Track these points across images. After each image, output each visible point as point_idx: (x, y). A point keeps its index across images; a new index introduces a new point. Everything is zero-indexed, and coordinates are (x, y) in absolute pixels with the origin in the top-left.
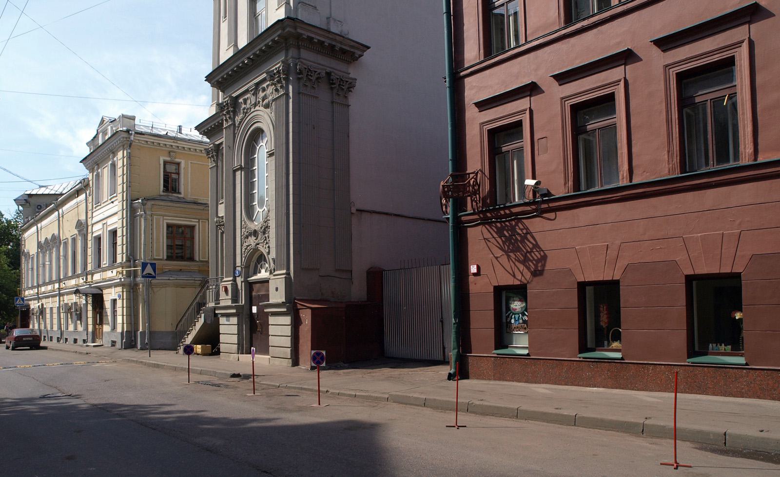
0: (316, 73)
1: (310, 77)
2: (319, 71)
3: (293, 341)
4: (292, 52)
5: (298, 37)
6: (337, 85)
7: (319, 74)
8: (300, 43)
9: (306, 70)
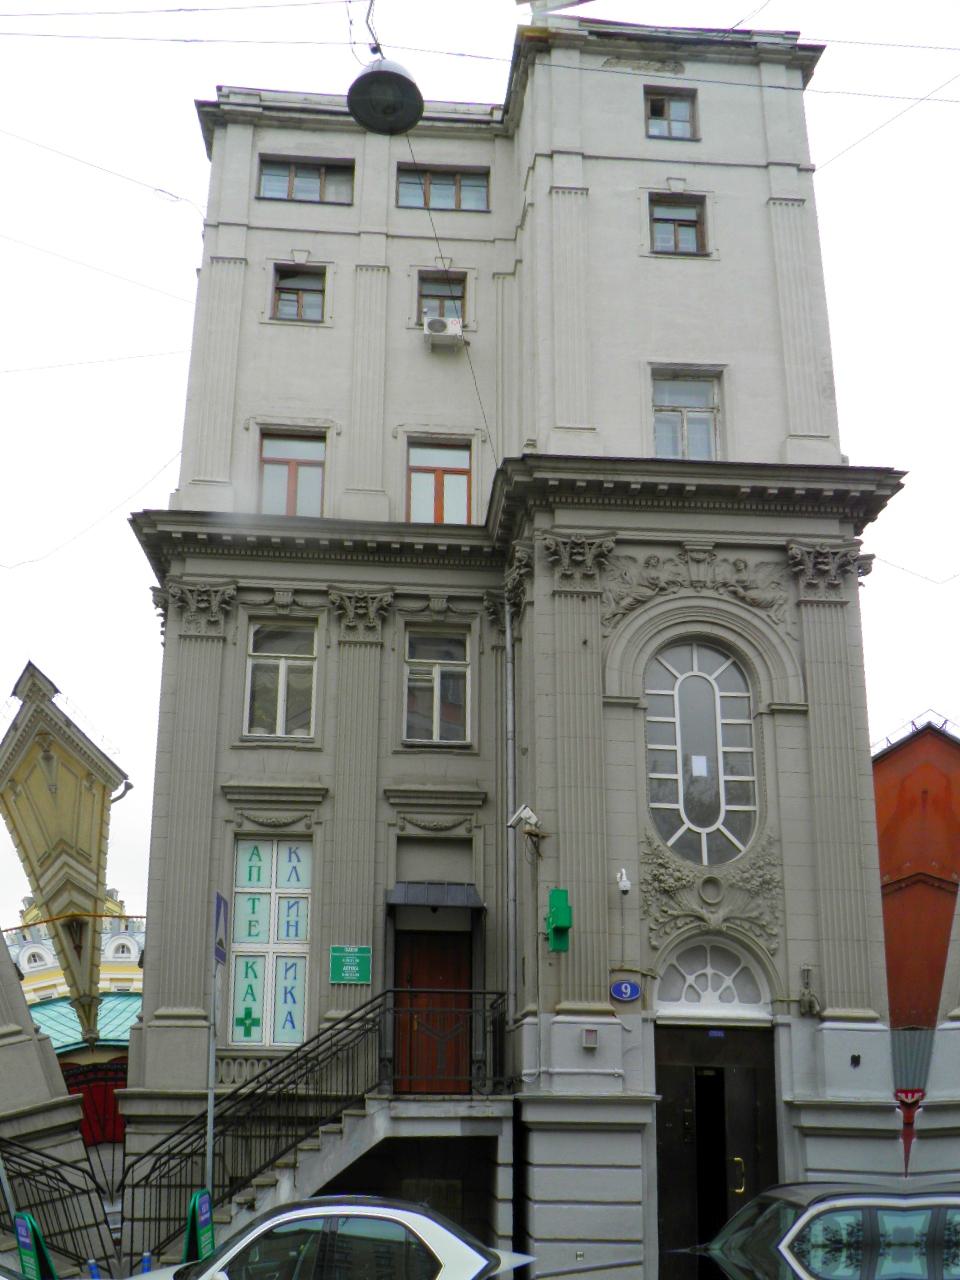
5: (542, 488)
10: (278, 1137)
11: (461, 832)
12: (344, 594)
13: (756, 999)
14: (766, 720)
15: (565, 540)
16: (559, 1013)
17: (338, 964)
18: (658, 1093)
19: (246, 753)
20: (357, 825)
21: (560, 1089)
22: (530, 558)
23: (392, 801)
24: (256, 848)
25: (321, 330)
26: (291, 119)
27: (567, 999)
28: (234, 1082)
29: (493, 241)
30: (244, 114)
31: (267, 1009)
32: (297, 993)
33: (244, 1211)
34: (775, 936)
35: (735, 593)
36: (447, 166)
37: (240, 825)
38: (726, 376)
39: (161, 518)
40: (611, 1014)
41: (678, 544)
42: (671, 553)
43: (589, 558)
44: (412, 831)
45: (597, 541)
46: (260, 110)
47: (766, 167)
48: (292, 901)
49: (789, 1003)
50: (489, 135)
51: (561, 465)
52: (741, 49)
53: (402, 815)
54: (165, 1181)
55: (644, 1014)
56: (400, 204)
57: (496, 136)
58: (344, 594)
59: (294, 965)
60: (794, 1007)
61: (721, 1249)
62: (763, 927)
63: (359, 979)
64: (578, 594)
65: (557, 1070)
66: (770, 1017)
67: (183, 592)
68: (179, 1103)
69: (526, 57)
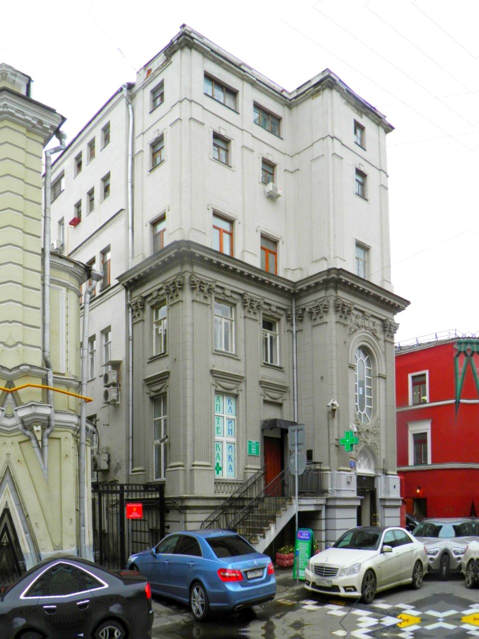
0: (208, 285)
1: (202, 288)
2: (210, 283)
3: (285, 444)
4: (187, 268)
6: (248, 304)
7: (210, 285)
8: (193, 260)
9: (199, 282)
10: (235, 514)
11: (280, 401)
12: (311, 307)
13: (370, 468)
14: (378, 379)
16: (339, 470)
17: (250, 450)
18: (401, 496)
19: (217, 356)
20: (252, 393)
21: (344, 495)
23: (263, 385)
24: (218, 397)
26: (219, 60)
29: (284, 154)
30: (202, 48)
31: (225, 465)
32: (233, 458)
33: (262, 538)
34: (275, 442)
35: (373, 333)
36: (266, 108)
37: (216, 387)
38: (370, 250)
40: (350, 471)
41: (363, 312)
42: (361, 314)
43: (205, 289)
46: (209, 50)
47: (380, 170)
48: (230, 421)
49: (380, 469)
50: (283, 103)
51: (347, 275)
52: (378, 118)
53: (217, 381)
55: (355, 472)
57: (286, 105)
59: (231, 446)
60: (382, 471)
61: (61, 570)
62: (376, 446)
63: (256, 454)
64: (343, 324)
65: (343, 489)
66: (375, 474)
67: (310, 309)
68: (212, 501)
69: (322, 86)
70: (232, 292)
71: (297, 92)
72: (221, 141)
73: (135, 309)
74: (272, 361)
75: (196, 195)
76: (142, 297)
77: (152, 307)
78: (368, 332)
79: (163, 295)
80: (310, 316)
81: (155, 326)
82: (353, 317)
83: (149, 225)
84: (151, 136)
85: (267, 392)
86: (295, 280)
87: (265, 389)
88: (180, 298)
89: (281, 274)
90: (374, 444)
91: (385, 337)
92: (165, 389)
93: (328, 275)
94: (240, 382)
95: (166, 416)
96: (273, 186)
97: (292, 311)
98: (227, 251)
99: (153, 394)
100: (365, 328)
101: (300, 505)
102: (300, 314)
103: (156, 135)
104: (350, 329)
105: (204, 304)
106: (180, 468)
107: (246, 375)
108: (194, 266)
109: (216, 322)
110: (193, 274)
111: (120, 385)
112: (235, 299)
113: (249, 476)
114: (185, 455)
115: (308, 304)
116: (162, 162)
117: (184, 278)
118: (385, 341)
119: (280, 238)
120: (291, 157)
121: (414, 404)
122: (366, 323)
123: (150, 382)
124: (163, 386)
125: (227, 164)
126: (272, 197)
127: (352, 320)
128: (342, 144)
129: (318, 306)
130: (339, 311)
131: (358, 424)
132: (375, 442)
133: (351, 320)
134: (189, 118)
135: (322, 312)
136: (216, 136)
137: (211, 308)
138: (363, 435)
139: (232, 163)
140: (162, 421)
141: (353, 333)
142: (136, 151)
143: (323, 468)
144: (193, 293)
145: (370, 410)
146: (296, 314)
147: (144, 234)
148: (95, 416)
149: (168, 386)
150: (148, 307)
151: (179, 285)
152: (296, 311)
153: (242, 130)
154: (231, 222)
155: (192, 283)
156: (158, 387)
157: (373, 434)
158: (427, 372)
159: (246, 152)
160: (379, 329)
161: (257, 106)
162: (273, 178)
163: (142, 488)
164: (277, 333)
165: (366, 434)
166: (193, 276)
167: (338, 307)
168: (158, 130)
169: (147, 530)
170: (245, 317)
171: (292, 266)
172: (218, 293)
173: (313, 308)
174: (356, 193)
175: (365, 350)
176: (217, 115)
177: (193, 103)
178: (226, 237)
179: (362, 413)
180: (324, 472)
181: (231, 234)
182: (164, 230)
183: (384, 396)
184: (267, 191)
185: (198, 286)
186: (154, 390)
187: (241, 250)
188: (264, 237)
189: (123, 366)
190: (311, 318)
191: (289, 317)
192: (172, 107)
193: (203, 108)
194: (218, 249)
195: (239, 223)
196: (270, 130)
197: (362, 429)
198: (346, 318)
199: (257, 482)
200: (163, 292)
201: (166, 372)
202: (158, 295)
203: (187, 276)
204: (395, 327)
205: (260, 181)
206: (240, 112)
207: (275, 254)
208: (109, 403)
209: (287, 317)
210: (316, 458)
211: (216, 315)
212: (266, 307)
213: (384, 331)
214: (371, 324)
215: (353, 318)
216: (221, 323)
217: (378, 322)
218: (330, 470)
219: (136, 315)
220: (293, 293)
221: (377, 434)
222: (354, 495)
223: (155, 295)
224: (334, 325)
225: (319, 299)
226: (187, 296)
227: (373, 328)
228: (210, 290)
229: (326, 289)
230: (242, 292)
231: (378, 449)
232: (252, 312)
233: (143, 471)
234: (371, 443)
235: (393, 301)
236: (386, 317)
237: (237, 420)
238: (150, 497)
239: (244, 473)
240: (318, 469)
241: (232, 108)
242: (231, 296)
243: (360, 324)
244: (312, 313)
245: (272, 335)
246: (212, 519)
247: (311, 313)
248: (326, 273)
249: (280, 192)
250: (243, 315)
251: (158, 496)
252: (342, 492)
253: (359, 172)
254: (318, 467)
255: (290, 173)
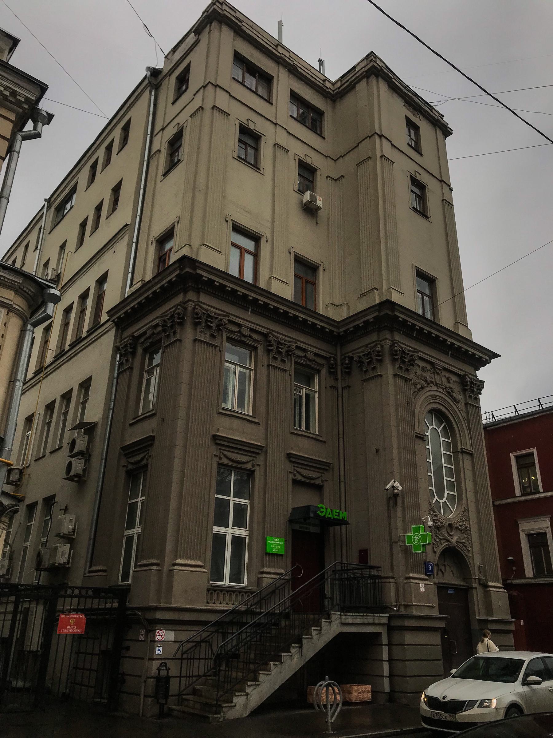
4: (191, 295)
6: (274, 348)
11: (318, 482)
12: (361, 354)
15: (205, 312)
22: (185, 314)
25: (256, 173)
27: (180, 558)
28: (233, 604)
29: (327, 157)
35: (449, 393)
37: (220, 459)
39: (201, 266)
42: (429, 367)
43: (214, 325)
44: (299, 477)
45: (220, 317)
53: (295, 468)
54: (185, 656)
56: (210, 84)
58: (361, 354)
62: (466, 547)
67: (360, 357)
70: (252, 330)
71: (341, 81)
72: (249, 137)
73: (125, 352)
74: (308, 427)
75: (246, 213)
76: (133, 336)
77: (145, 351)
78: (441, 390)
79: (158, 333)
80: (359, 367)
81: (145, 376)
82: (418, 369)
83: (154, 243)
84: (170, 132)
85: (299, 470)
86: (338, 319)
87: (296, 465)
88: (178, 336)
89: (321, 310)
90: (462, 543)
91: (466, 400)
92: (147, 460)
93: (379, 311)
94: (258, 454)
95: (144, 498)
96: (311, 196)
97: (335, 360)
98: (248, 277)
99: (130, 467)
100: (437, 385)
101: (344, 624)
102: (347, 364)
103: (175, 131)
104: (415, 384)
105: (211, 345)
106: (155, 568)
107: (267, 445)
108: (201, 293)
109: (228, 370)
110: (198, 303)
111: (90, 456)
112: (255, 341)
113: (265, 583)
114: (163, 550)
115: (356, 351)
116: (179, 161)
117: (186, 309)
118: (466, 404)
119: (321, 263)
120: (335, 161)
121: (522, 495)
122: (438, 379)
123: (129, 451)
124: (145, 455)
125: (256, 166)
126: (310, 210)
127: (416, 374)
128: (392, 145)
129: (370, 352)
130: (397, 359)
131: (435, 516)
132: (464, 541)
133: (416, 373)
134: (212, 106)
135: (374, 361)
136: (244, 130)
137: (220, 351)
138: (444, 532)
139: (261, 165)
140: (140, 505)
141: (419, 390)
142: (154, 150)
143: (382, 574)
144: (196, 330)
145: (451, 498)
146: (342, 364)
147: (149, 255)
148: (54, 496)
149: (150, 456)
150: (140, 350)
151: (179, 318)
152: (341, 361)
153: (276, 124)
154: (256, 238)
155: (195, 316)
156: (138, 458)
157: (459, 529)
158: (535, 451)
159: (278, 150)
160: (456, 388)
161: (295, 97)
162: (313, 187)
163: (90, 593)
164: (317, 389)
165: (449, 530)
166: (197, 307)
167: (397, 355)
168: (178, 124)
169: (97, 651)
170: (269, 366)
171: (334, 300)
172: (232, 332)
173: (363, 355)
174: (413, 208)
175: (440, 415)
176: (242, 104)
177: (217, 87)
178: (249, 260)
179: (441, 501)
180: (383, 580)
181: (256, 255)
182: (171, 250)
183: (471, 479)
184: (304, 201)
185: (202, 321)
186: (132, 461)
187: (267, 276)
188: (299, 261)
189: (99, 430)
190: (362, 370)
191: (333, 368)
192: (194, 95)
193: (230, 95)
194: (237, 275)
195: (267, 241)
196: (310, 127)
197: (442, 523)
198: (407, 370)
199: (277, 591)
200: (160, 329)
201: (151, 436)
202: (153, 334)
203: (190, 305)
204: (479, 386)
205: (296, 188)
206: (274, 102)
207: (314, 284)
208: (70, 479)
209: (330, 368)
210: (373, 562)
211: (226, 361)
212: (301, 354)
213: (464, 391)
214: (444, 380)
215: (419, 371)
216: (234, 373)
217: (454, 378)
218: (393, 578)
219: (124, 361)
220: (337, 335)
221: (465, 531)
222: (435, 613)
223: (149, 333)
224: (391, 380)
225: (369, 344)
226: (188, 334)
227: (448, 385)
228: (220, 327)
229: (379, 330)
230: (265, 331)
231: (468, 551)
232: (279, 359)
233: (105, 571)
234: (456, 542)
235: (471, 351)
236: (268, 329)
237: (251, 506)
238: (109, 605)
239: (258, 578)
240: (374, 576)
241: (266, 98)
242: (250, 336)
243: (429, 379)
244: (363, 362)
245: (309, 392)
246: (198, 639)
247: (361, 362)
248: (177, 265)
249: (320, 203)
250: (266, 363)
251: (116, 605)
252: (414, 607)
253: (415, 182)
254: (374, 573)
255: (333, 181)
